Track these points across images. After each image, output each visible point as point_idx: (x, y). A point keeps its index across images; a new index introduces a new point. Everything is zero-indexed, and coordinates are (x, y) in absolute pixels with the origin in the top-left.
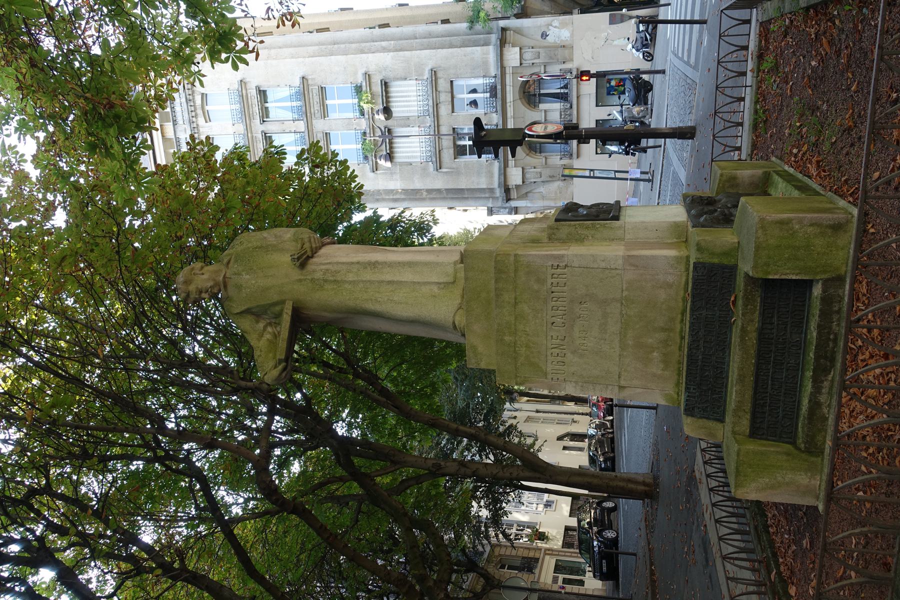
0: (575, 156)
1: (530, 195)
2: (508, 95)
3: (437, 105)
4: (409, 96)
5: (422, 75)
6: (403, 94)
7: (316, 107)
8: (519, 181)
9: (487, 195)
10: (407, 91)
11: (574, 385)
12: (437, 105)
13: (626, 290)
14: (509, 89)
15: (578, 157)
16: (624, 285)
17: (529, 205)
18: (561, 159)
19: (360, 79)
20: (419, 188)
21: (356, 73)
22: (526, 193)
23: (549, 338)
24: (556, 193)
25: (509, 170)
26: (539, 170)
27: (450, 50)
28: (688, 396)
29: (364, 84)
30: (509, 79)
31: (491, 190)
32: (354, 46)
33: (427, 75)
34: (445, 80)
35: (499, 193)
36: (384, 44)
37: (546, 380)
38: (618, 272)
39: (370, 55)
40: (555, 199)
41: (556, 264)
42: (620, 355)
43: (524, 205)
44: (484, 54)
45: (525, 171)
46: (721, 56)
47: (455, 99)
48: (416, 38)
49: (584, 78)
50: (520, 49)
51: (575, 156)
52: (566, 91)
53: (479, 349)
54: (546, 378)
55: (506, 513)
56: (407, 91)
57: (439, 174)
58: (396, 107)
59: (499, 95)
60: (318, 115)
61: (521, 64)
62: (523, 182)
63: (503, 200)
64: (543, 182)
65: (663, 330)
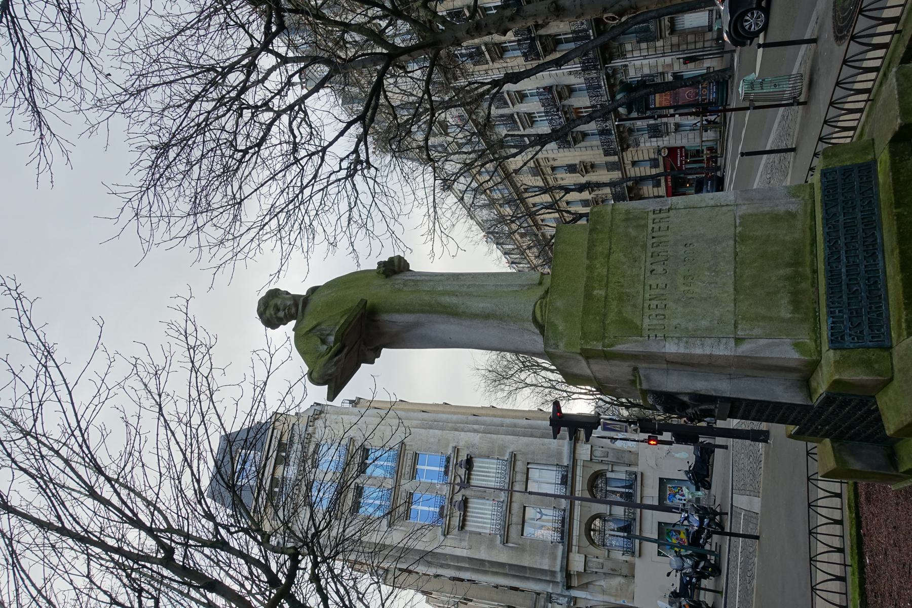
0: (637, 553)
1: (591, 586)
2: (577, 484)
3: (513, 483)
4: (489, 472)
5: (504, 455)
6: (479, 511)
7: (407, 469)
8: (581, 569)
9: (548, 578)
10: (487, 468)
11: (676, 341)
12: (513, 483)
13: (740, 226)
14: (579, 479)
15: (640, 556)
16: (738, 221)
17: (589, 597)
18: (623, 554)
19: (450, 451)
20: (484, 558)
21: (447, 446)
22: (587, 584)
23: (647, 288)
24: (617, 589)
25: (571, 555)
26: (601, 561)
27: (531, 439)
28: (833, 322)
29: (452, 455)
30: (579, 471)
31: (553, 573)
32: (450, 425)
33: (507, 457)
34: (523, 462)
35: (559, 578)
36: (476, 427)
37: (641, 339)
38: (730, 208)
39: (463, 433)
40: (616, 596)
41: (658, 208)
42: (735, 300)
43: (584, 597)
44: (559, 446)
45: (588, 559)
46: (823, 134)
47: (529, 481)
48: (503, 426)
49: (652, 442)
50: (592, 447)
51: (637, 553)
52: (631, 491)
53: (560, 328)
54: (641, 336)
55: (623, 55)
56: (487, 468)
57: (505, 548)
58: (474, 475)
59: (569, 483)
60: (407, 476)
61: (591, 459)
62: (585, 570)
63: (563, 586)
64: (605, 574)
65: (789, 265)
